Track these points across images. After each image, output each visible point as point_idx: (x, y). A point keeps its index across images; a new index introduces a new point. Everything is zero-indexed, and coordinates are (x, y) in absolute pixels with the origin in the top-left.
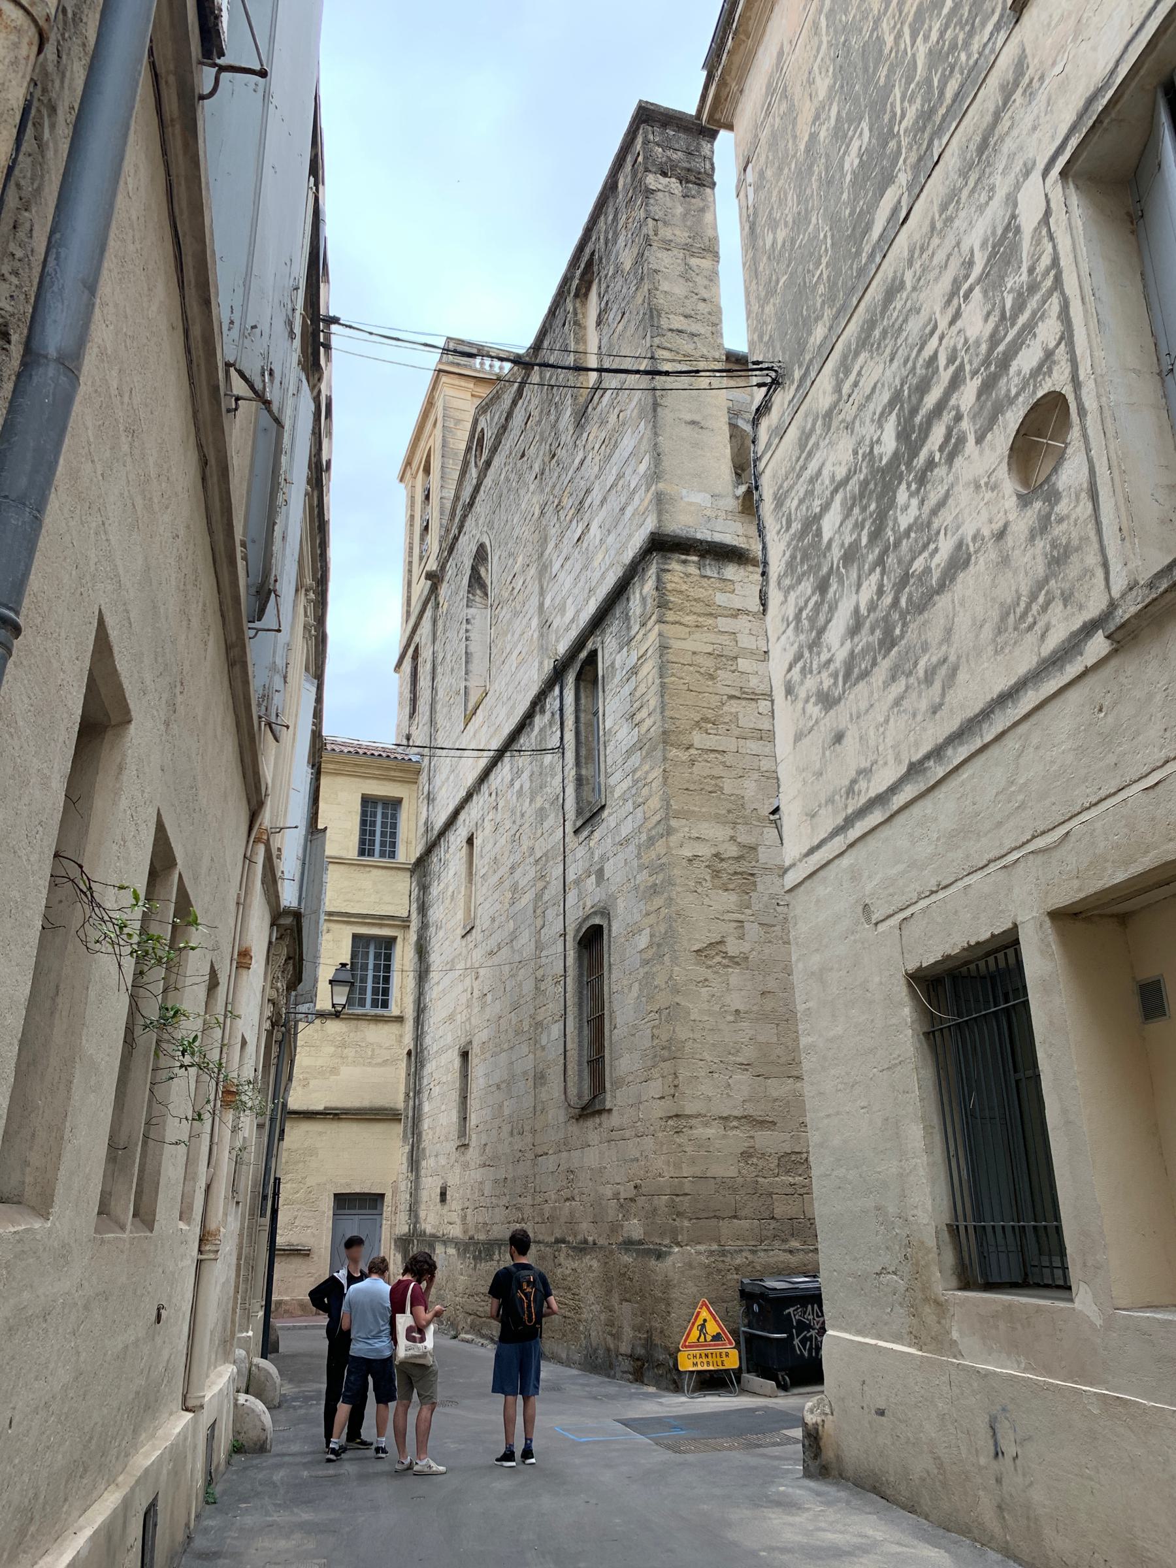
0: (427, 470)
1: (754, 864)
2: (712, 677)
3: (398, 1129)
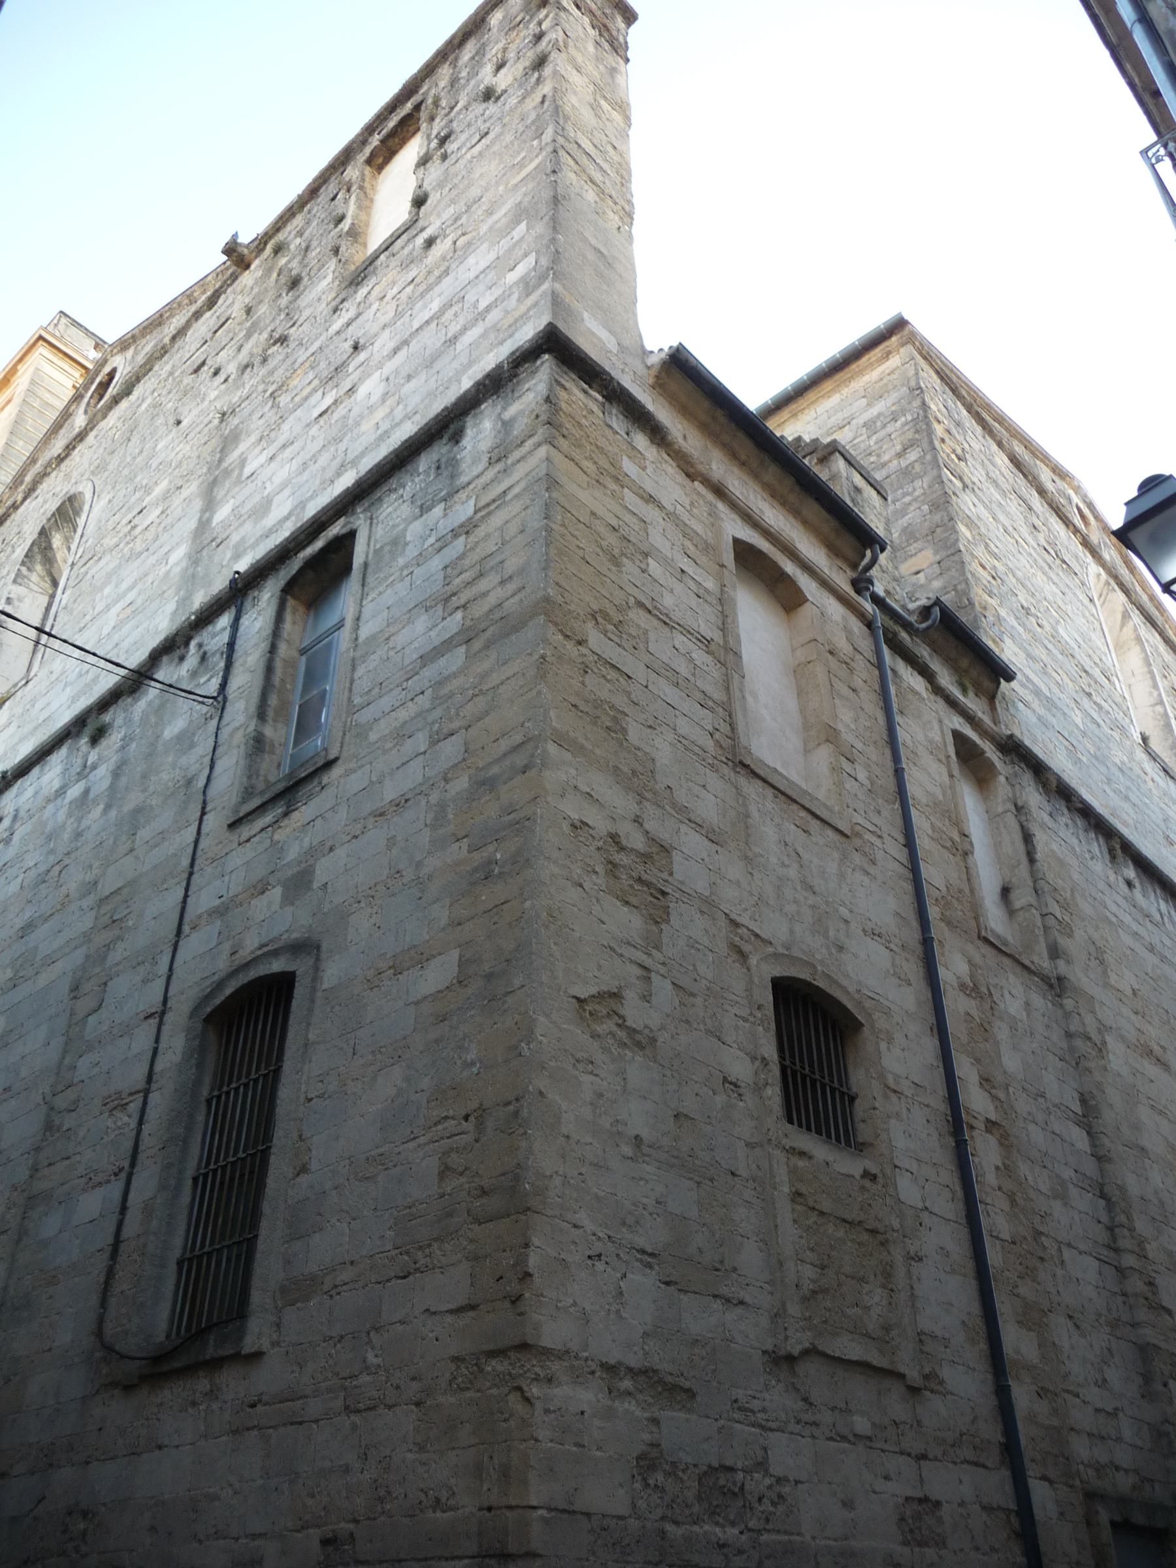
1: (665, 876)
2: (615, 561)
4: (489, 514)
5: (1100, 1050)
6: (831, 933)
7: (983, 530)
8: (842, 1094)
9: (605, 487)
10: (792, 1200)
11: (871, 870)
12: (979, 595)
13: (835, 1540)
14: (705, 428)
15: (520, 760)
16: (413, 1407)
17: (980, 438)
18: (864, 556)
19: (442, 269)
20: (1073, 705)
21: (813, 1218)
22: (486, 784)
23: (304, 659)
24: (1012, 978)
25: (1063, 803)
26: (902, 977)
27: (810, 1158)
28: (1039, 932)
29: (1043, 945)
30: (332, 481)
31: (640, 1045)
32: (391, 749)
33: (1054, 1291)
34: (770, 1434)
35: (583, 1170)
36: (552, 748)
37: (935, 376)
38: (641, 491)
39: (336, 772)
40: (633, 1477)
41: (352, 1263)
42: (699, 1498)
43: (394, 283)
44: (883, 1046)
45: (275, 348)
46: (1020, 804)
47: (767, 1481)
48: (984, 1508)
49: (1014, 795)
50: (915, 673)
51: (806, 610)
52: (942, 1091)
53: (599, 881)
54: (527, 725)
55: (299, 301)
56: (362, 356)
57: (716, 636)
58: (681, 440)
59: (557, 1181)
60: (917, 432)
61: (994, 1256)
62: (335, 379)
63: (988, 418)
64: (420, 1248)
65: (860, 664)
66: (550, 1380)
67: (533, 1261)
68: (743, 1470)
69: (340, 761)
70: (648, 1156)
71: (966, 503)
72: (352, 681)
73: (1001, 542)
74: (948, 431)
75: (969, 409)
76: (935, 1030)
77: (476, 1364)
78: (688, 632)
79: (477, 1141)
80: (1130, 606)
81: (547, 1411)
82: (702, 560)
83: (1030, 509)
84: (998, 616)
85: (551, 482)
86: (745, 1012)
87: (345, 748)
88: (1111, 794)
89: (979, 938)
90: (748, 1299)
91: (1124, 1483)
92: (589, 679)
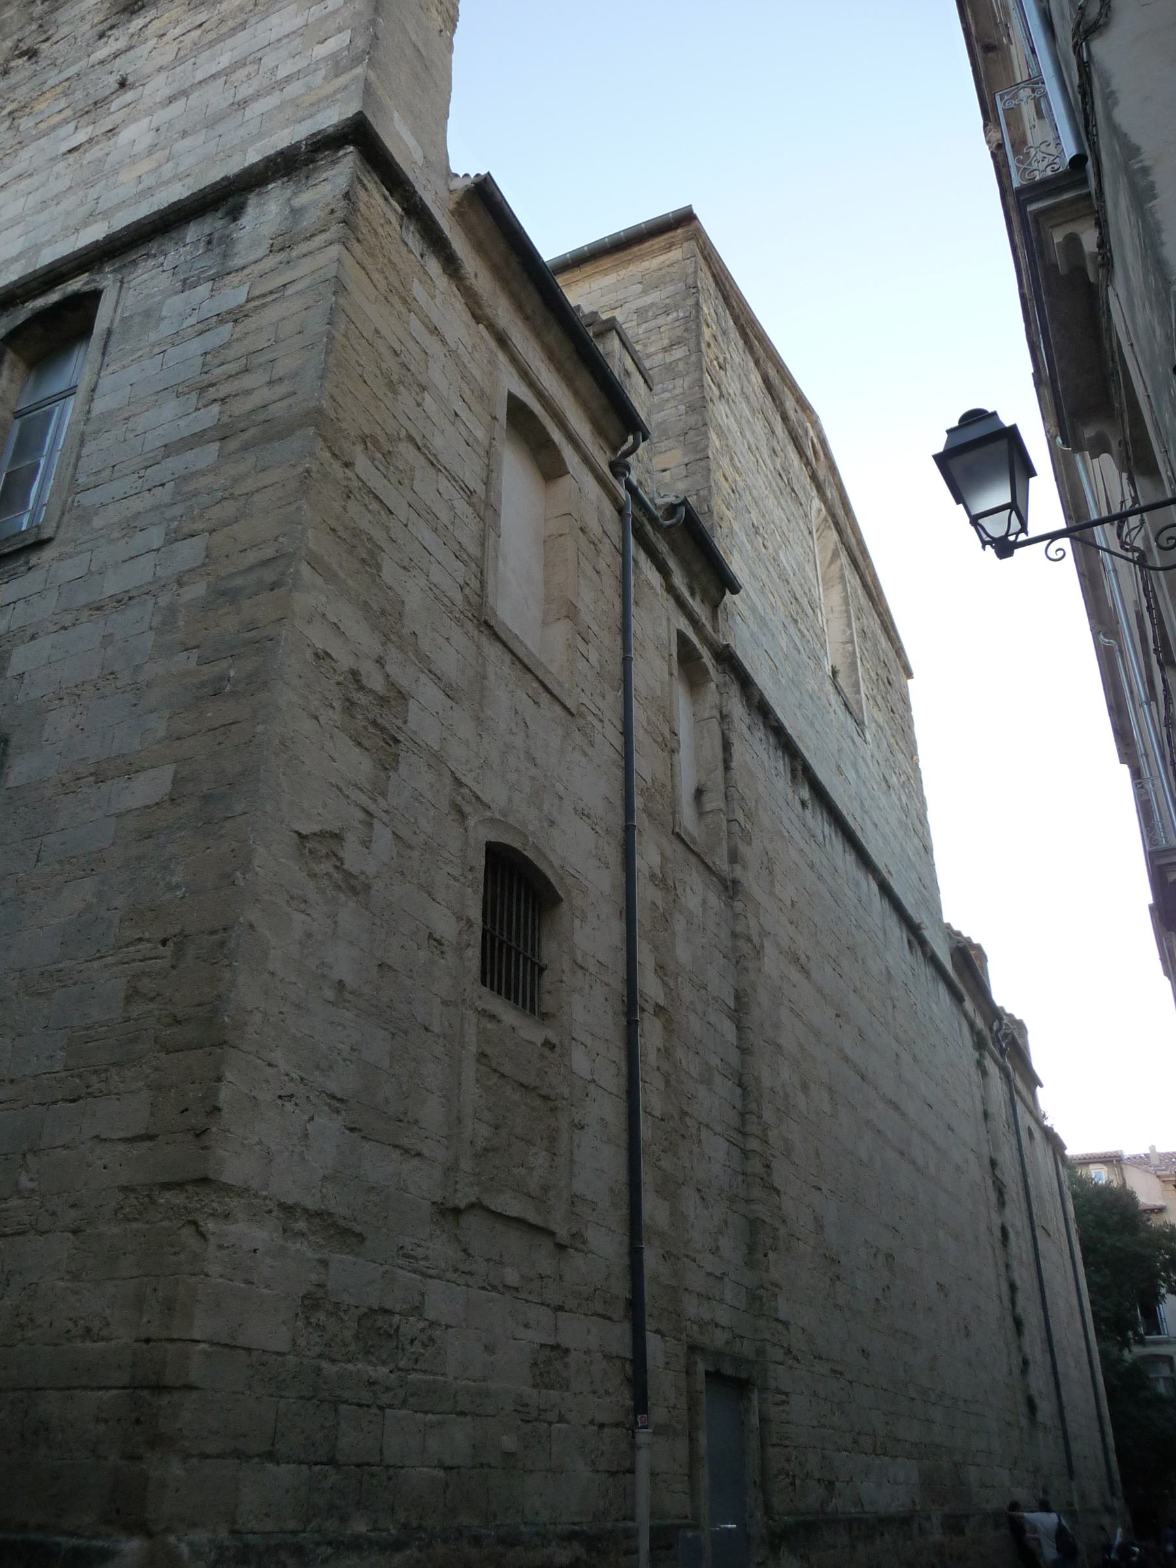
1: (399, 723)
2: (391, 385)
4: (264, 305)
5: (758, 952)
6: (545, 807)
7: (731, 442)
8: (533, 964)
9: (392, 306)
10: (478, 1061)
11: (590, 751)
12: (718, 505)
13: (474, 1381)
14: (496, 271)
15: (269, 576)
16: (70, 1235)
17: (741, 351)
18: (626, 441)
19: (239, 20)
20: (781, 628)
21: (495, 1079)
22: (225, 595)
23: (17, 423)
24: (695, 874)
25: (761, 719)
26: (603, 859)
27: (499, 1021)
28: (723, 835)
29: (725, 847)
30: (77, 230)
31: (354, 891)
32: (118, 539)
33: (688, 1165)
34: (430, 1281)
35: (284, 1010)
36: (305, 570)
37: (711, 280)
38: (427, 321)
39: (48, 554)
40: (297, 1315)
41: (12, 1081)
42: (357, 1337)
43: (178, 22)
44: (577, 922)
45: (20, 61)
46: (724, 712)
47: (421, 1325)
48: (605, 1356)
49: (721, 704)
50: (654, 568)
51: (565, 481)
52: (622, 973)
53: (335, 718)
54: (281, 539)
55: (57, 15)
56: (129, 96)
57: (480, 488)
58: (473, 280)
59: (258, 1017)
60: (686, 330)
61: (646, 1131)
62: (93, 115)
63: (751, 334)
64: (96, 1072)
65: (606, 547)
66: (227, 1216)
67: (224, 1095)
68: (400, 1314)
69: (54, 543)
70: (349, 1002)
71: (720, 411)
72: (79, 457)
73: (746, 460)
74: (714, 337)
75: (736, 320)
76: (624, 913)
77: (148, 1195)
78: (453, 478)
79: (173, 967)
80: (840, 546)
81: (221, 1247)
82: (477, 407)
83: (773, 432)
84: (731, 529)
85: (340, 287)
86: (456, 872)
87: (62, 530)
88: (800, 717)
89: (673, 833)
90: (425, 1152)
91: (719, 1339)
92: (352, 506)
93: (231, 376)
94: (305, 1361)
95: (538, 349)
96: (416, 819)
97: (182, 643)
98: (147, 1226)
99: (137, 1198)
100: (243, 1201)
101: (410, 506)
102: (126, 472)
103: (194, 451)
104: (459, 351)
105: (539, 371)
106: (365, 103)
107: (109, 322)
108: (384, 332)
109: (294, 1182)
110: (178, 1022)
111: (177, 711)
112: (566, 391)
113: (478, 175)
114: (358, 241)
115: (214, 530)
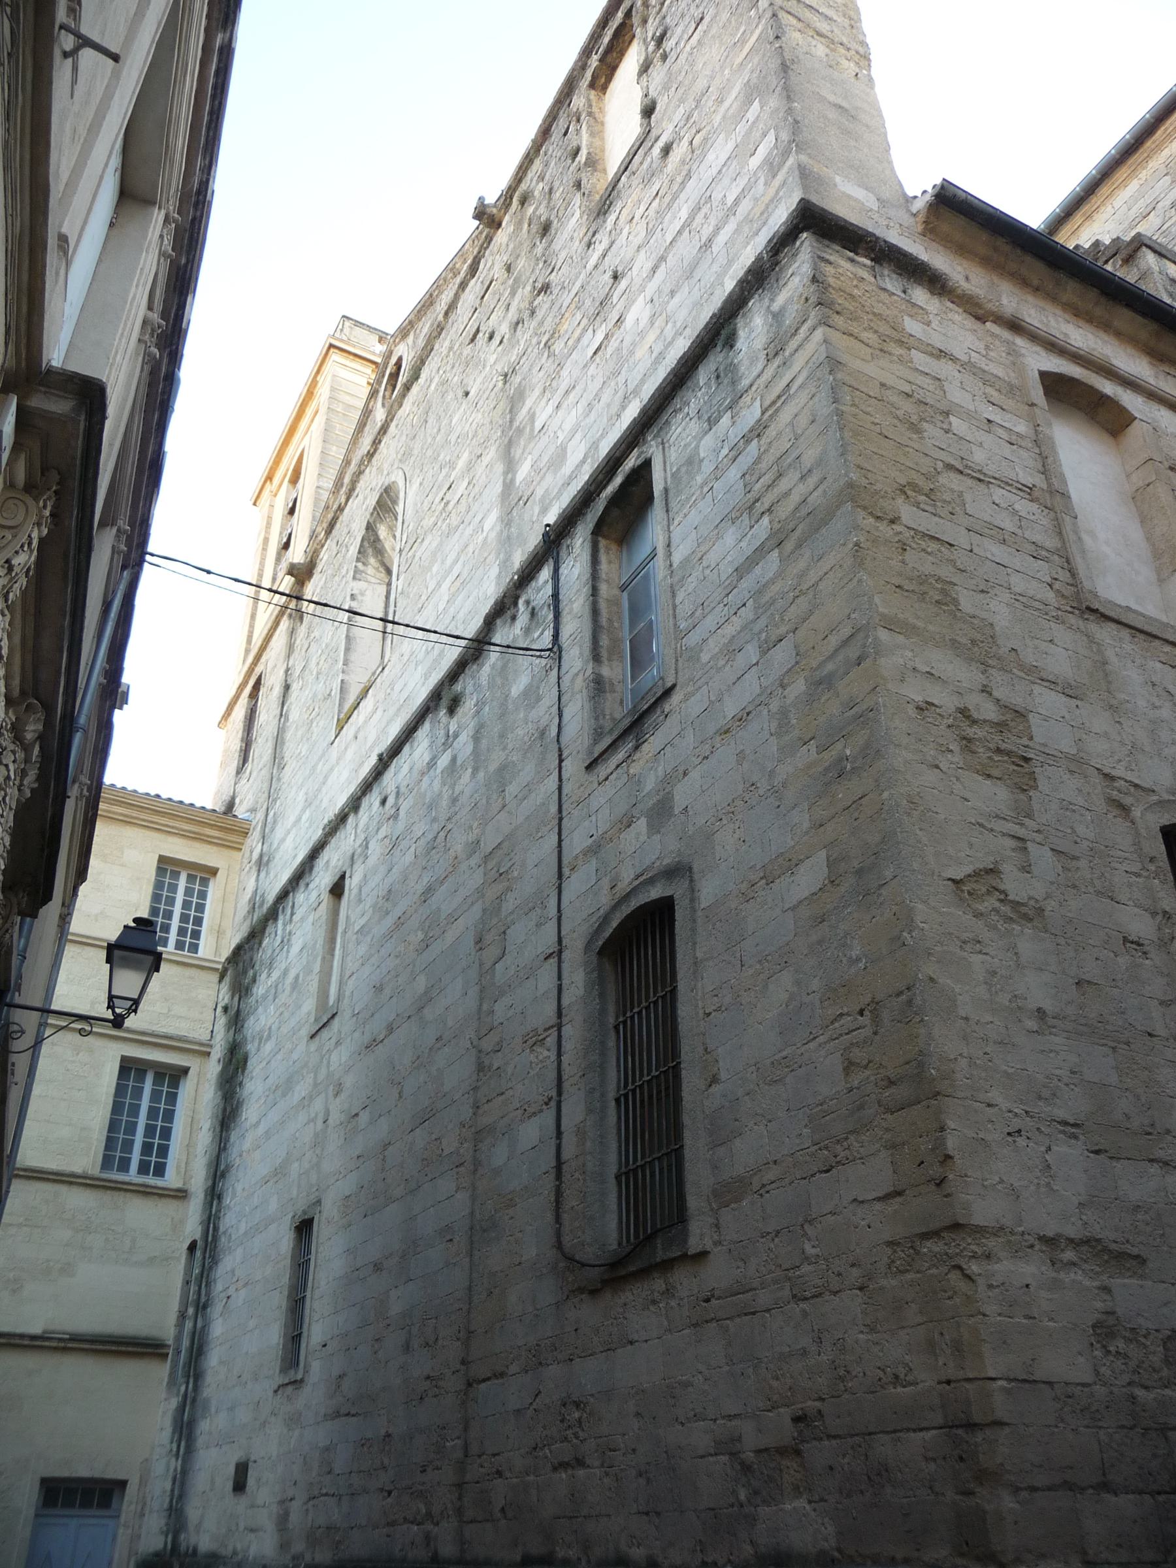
0: (295, 479)
1: (1025, 741)
2: (915, 428)
3: (161, 1371)
4: (777, 411)
15: (853, 652)
16: (858, 1291)
19: (684, 173)
22: (822, 683)
30: (619, 416)
31: (1027, 918)
35: (988, 1050)
36: (883, 635)
38: (930, 349)
39: (676, 698)
41: (775, 1162)
43: (640, 201)
45: (540, 298)
51: (1135, 429)
54: (853, 616)
56: (623, 284)
59: (963, 1063)
62: (602, 314)
67: (952, 1144)
69: (678, 687)
72: (675, 607)
77: (912, 1247)
78: (1005, 483)
79: (875, 1033)
81: (990, 1286)
82: (1009, 404)
92: (910, 556)
93: (769, 486)
94: (1115, 1390)
95: (1059, 312)
96: (1072, 828)
97: (800, 739)
98: (919, 1275)
99: (903, 1251)
100: (1000, 1240)
101: (969, 530)
102: (713, 605)
103: (760, 565)
104: (972, 360)
105: (1066, 334)
106: (805, 187)
107: (663, 482)
108: (889, 382)
109: (1049, 1214)
110: (891, 1083)
111: (814, 801)
112: (1105, 337)
113: (934, 186)
114: (838, 313)
115: (796, 628)
